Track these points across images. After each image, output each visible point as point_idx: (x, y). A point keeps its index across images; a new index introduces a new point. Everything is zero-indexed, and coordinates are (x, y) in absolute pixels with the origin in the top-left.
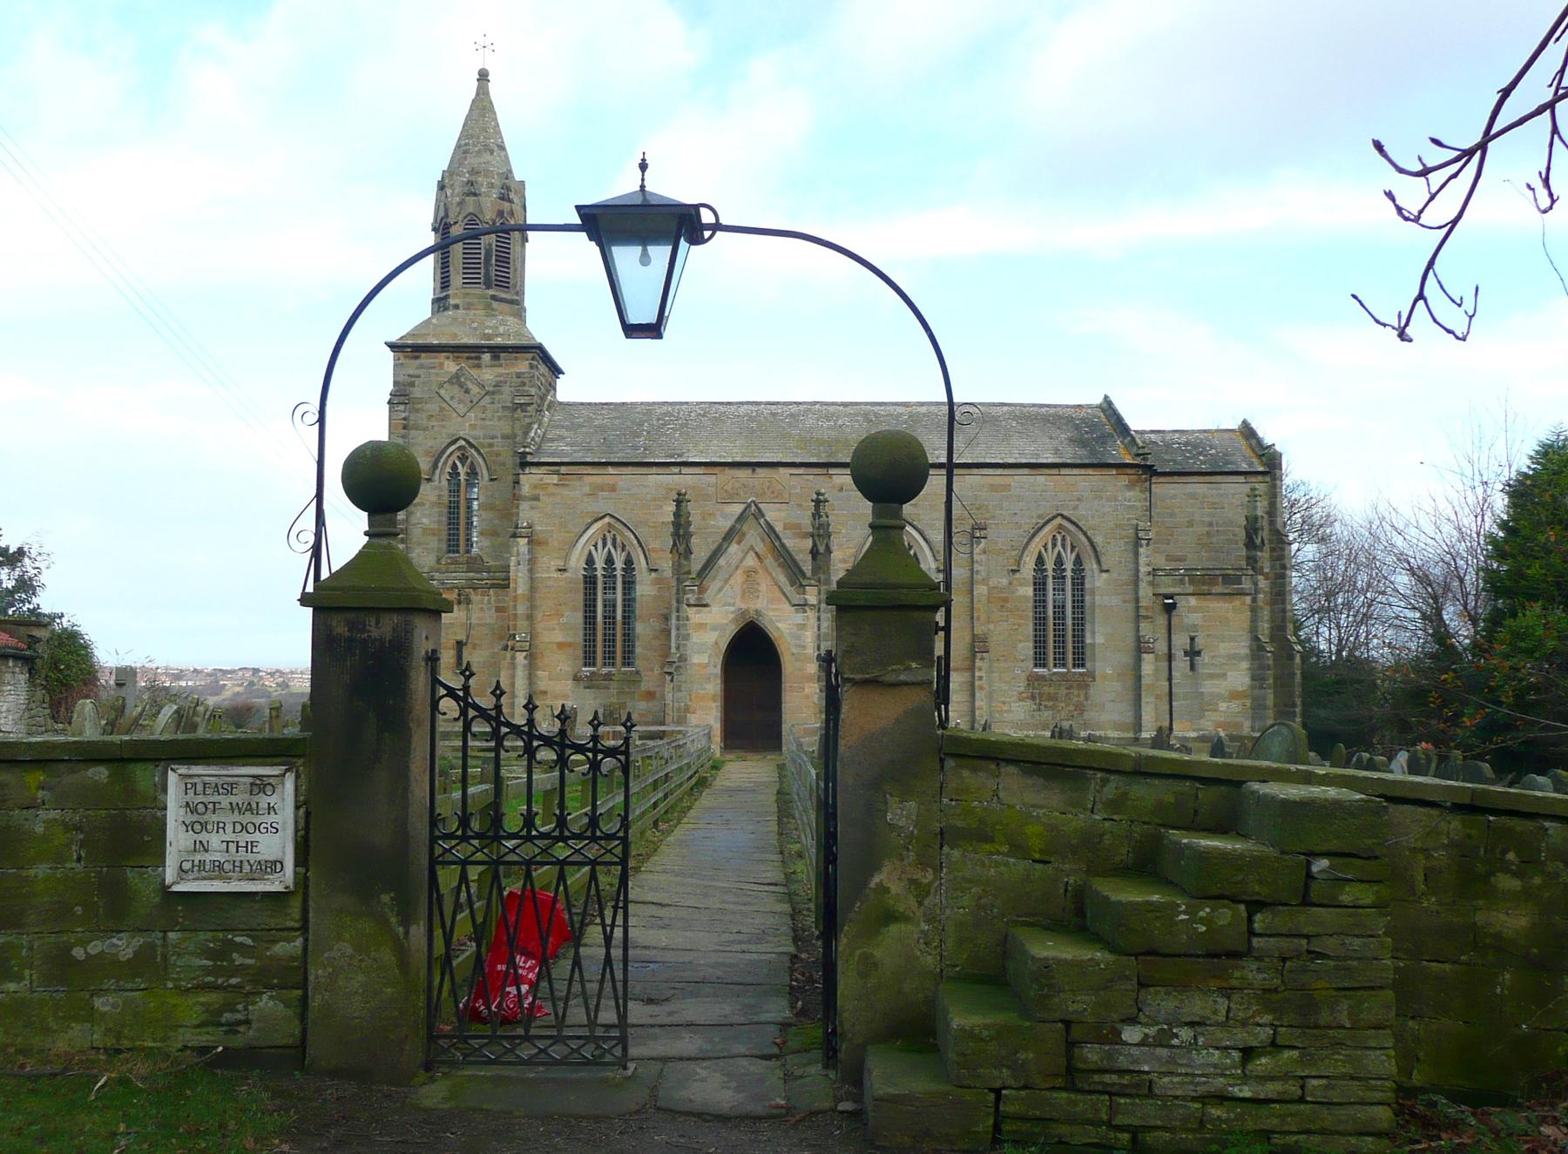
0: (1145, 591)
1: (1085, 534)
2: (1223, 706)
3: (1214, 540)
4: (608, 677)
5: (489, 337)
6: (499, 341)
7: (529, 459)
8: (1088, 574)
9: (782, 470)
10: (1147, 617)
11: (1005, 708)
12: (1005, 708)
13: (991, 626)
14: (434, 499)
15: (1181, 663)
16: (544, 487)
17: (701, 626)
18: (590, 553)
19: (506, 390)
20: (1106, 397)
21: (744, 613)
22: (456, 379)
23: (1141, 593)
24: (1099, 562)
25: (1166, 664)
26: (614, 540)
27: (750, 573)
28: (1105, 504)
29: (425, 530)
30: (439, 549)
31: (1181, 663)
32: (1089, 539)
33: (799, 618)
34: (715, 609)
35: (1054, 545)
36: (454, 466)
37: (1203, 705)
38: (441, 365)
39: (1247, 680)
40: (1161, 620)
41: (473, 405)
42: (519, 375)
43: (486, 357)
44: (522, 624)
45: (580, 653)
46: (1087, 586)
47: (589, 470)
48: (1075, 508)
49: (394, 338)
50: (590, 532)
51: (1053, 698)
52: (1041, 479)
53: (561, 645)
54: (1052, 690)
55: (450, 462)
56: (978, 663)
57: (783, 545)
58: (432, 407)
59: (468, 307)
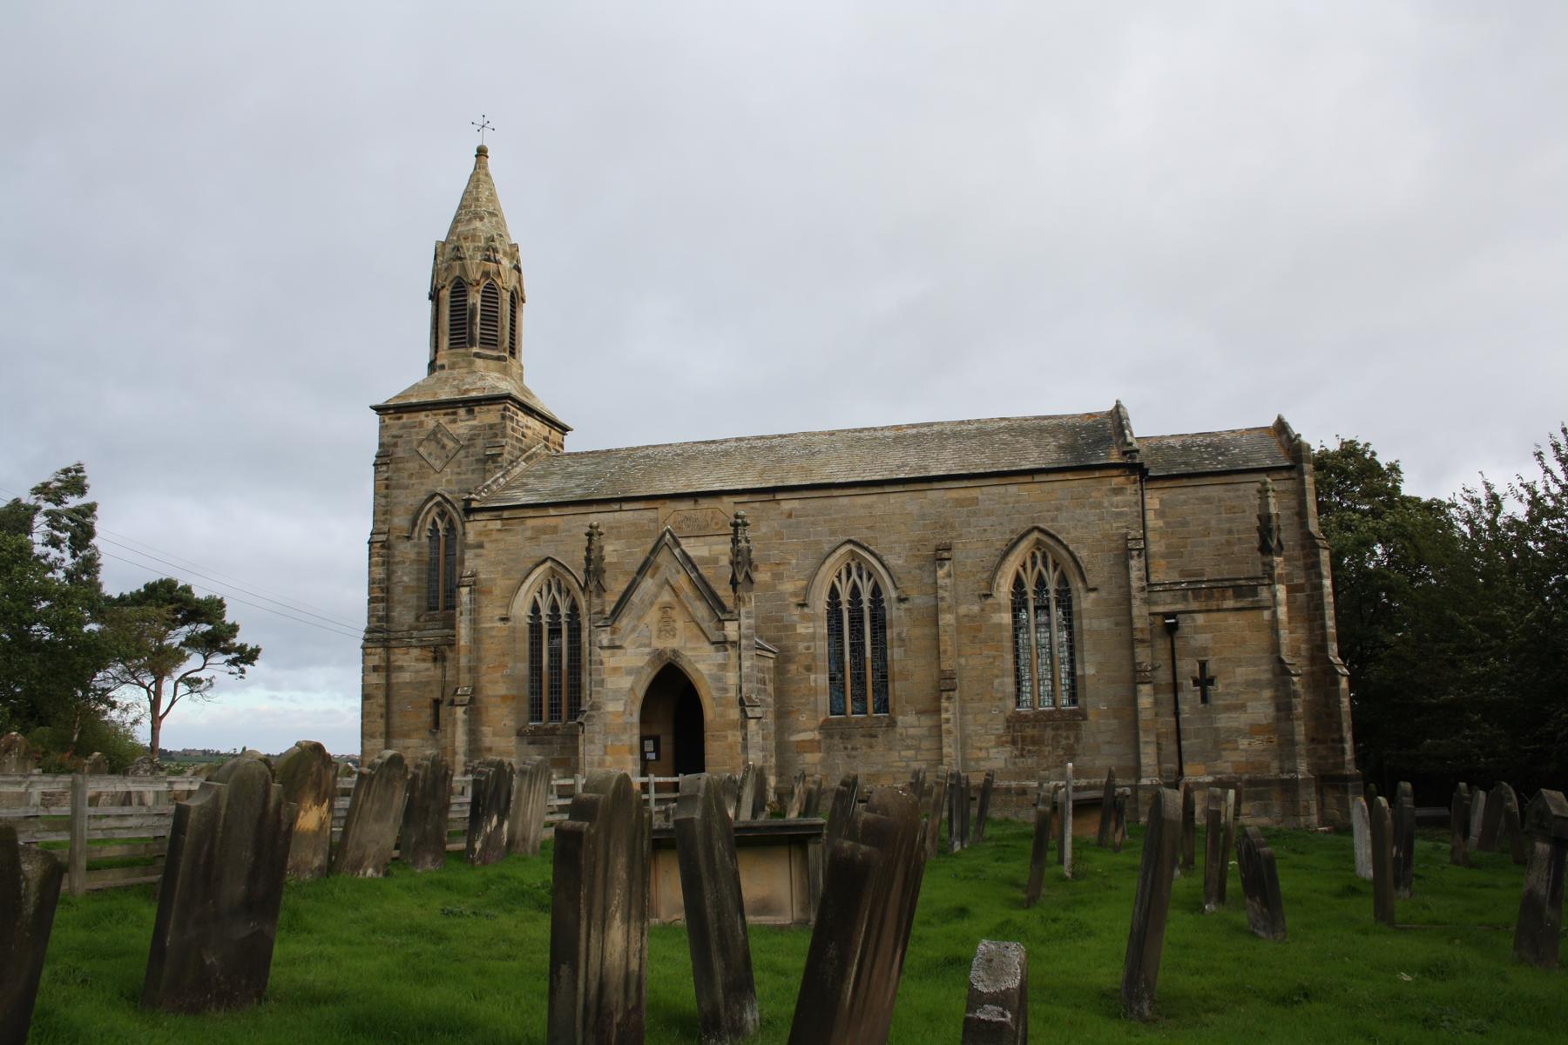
0: (1139, 609)
1: (1066, 548)
2: (1243, 743)
3: (1236, 549)
4: (553, 731)
5: (467, 391)
6: (474, 394)
7: (474, 505)
8: (1074, 594)
9: (726, 499)
10: (1142, 641)
11: (983, 754)
12: (983, 754)
13: (963, 661)
14: (413, 556)
15: (1189, 694)
16: (488, 533)
17: (615, 670)
18: (535, 601)
19: (480, 442)
20: (1118, 406)
21: (659, 654)
22: (434, 435)
23: (1135, 612)
24: (1084, 580)
25: (1170, 696)
26: (559, 584)
27: (665, 608)
28: (1089, 516)
29: (405, 587)
30: (419, 607)
31: (1189, 694)
32: (1071, 554)
33: (719, 657)
34: (631, 650)
35: (1034, 564)
36: (434, 523)
37: (1219, 743)
38: (421, 423)
39: (1271, 711)
40: (1162, 645)
41: (448, 460)
42: (491, 426)
43: (462, 412)
44: (465, 677)
45: (526, 706)
46: (1075, 609)
47: (531, 513)
48: (1054, 520)
49: (380, 402)
50: (532, 578)
51: (1035, 741)
52: (1013, 489)
53: (504, 698)
54: (1036, 732)
55: (429, 519)
56: (945, 704)
57: (700, 576)
58: (413, 466)
59: (453, 366)
